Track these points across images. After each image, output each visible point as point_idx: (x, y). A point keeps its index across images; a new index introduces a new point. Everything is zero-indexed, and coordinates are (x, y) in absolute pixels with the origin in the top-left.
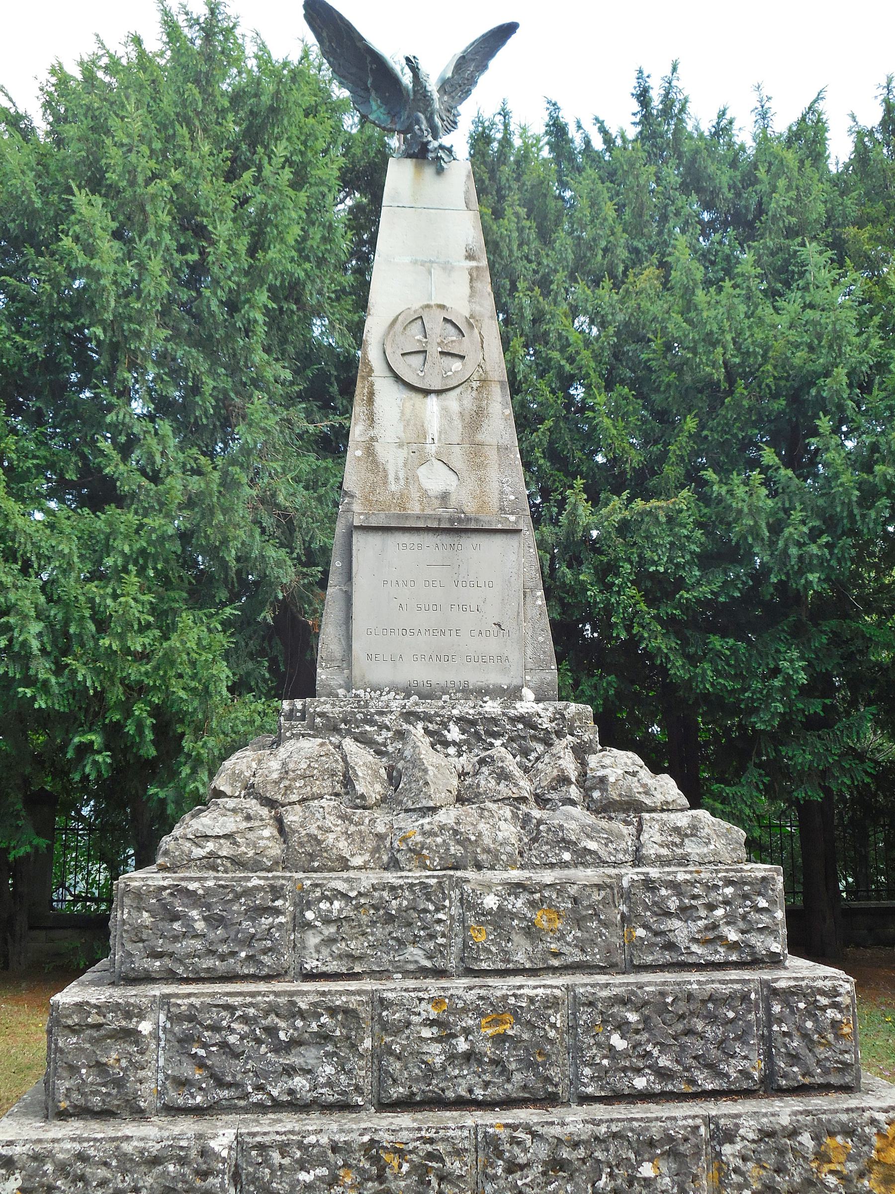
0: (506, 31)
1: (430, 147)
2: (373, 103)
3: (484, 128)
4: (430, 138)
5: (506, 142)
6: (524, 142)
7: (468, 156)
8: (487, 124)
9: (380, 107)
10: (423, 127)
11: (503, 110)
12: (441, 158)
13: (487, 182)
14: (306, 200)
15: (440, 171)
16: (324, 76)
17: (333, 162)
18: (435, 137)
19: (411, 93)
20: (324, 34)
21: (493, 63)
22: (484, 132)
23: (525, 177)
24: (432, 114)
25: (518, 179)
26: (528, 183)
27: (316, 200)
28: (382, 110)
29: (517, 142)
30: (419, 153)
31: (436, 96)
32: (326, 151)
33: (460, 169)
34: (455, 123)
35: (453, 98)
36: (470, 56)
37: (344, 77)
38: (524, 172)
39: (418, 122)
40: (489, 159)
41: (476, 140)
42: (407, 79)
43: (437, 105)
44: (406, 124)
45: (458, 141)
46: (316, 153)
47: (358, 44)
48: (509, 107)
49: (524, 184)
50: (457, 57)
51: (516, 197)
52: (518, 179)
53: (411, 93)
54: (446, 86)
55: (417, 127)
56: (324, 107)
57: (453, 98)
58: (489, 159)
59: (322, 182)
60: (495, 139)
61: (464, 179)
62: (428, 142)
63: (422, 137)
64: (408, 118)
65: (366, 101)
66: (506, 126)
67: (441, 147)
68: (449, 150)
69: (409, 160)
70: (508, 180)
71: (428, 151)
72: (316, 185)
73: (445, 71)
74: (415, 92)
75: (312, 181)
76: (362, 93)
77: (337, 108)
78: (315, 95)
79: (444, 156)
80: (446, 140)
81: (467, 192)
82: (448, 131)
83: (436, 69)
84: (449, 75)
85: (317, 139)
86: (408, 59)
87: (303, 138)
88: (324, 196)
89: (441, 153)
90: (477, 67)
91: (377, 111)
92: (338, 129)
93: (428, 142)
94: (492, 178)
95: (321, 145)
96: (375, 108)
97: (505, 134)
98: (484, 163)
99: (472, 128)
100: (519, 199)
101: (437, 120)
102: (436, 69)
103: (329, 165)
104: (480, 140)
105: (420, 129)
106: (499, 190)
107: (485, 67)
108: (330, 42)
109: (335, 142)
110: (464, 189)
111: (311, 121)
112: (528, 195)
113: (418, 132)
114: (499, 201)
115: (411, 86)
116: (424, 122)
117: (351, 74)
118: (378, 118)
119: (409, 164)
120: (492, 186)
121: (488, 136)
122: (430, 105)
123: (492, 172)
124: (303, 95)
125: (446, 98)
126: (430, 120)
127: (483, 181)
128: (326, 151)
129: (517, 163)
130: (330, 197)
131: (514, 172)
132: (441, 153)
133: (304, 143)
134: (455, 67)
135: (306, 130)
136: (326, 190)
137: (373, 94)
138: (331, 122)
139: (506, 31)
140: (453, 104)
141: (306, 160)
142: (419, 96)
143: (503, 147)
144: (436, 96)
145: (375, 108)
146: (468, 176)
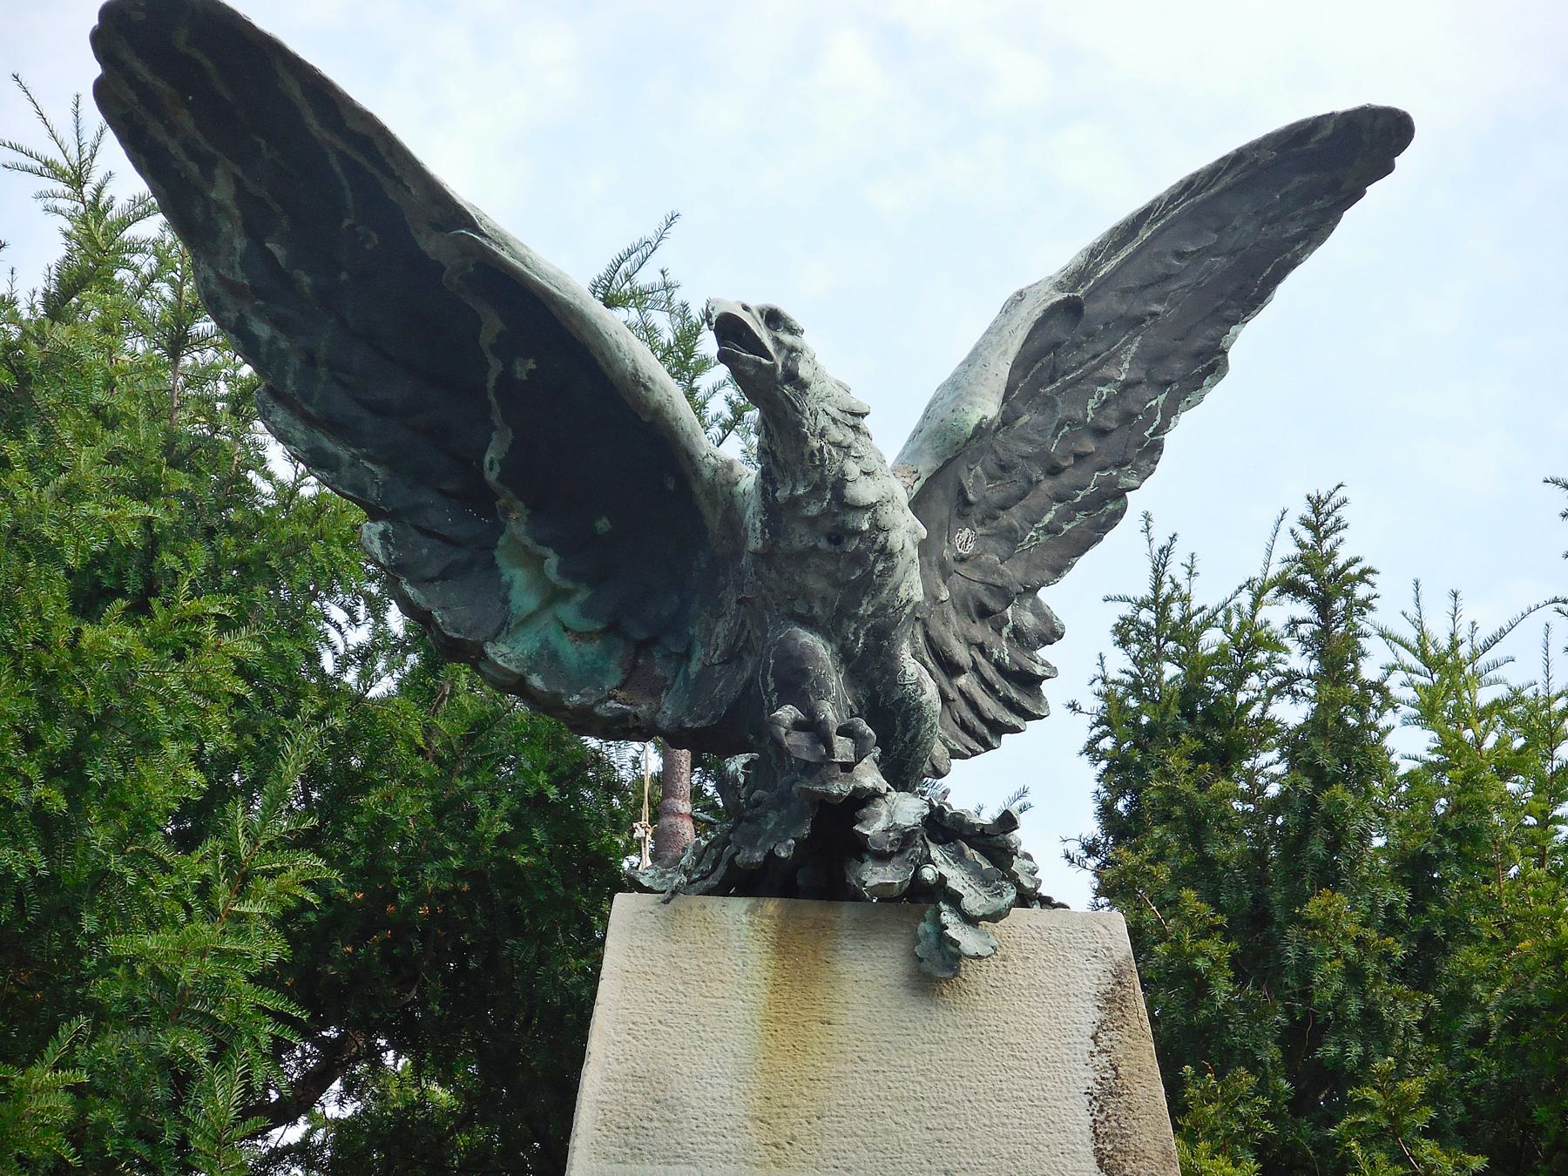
0: (1345, 154)
1: (874, 827)
2: (517, 577)
3: (1196, 667)
4: (869, 776)
5: (1338, 745)
6: (1450, 747)
7: (1092, 828)
8: (1212, 639)
9: (554, 596)
10: (830, 713)
11: (1312, 560)
12: (941, 892)
13: (1222, 989)
14: (63, 1105)
15: (936, 971)
16: (205, 374)
17: (242, 884)
18: (905, 769)
19: (752, 516)
20: (222, 192)
21: (1249, 344)
22: (1190, 692)
23: (1467, 957)
24: (882, 636)
25: (1419, 971)
26: (1492, 997)
27: (134, 1106)
28: (568, 612)
29: (1408, 744)
30: (806, 861)
31: (905, 530)
32: (197, 822)
33: (1062, 961)
34: (1030, 682)
35: (1011, 537)
36: (1110, 304)
37: (335, 427)
38: (1459, 930)
39: (795, 681)
40: (1227, 851)
41: (1147, 737)
42: (733, 452)
43: (912, 585)
44: (724, 690)
45: (1043, 783)
46: (141, 826)
47: (431, 245)
48: (1347, 549)
49: (1459, 1000)
50: (1031, 312)
51: (1413, 1086)
52: (1419, 971)
53: (752, 516)
54: (955, 469)
55: (787, 713)
56: (200, 555)
57: (1011, 537)
58: (1227, 851)
59: (173, 1002)
60: (1267, 727)
61: (1088, 1015)
62: (864, 799)
63: (822, 766)
64: (733, 657)
65: (472, 564)
66: (1335, 654)
67: (942, 827)
68: (993, 844)
69: (738, 907)
70: (1354, 974)
71: (860, 849)
72: (133, 1016)
73: (957, 388)
74: (776, 512)
75: (109, 991)
76: (441, 517)
77: (267, 567)
78: (145, 491)
79: (956, 879)
80: (972, 787)
81: (1107, 1095)
82: (984, 734)
83: (899, 364)
84: (987, 407)
85: (148, 744)
86: (730, 329)
87: (59, 738)
88: (181, 1078)
89: (941, 866)
90: (1153, 359)
91: (537, 624)
92: (282, 685)
93: (864, 799)
94: (1255, 963)
95: (172, 776)
96: (524, 599)
97: (1325, 706)
98: (1202, 873)
99: (1120, 663)
100: (1434, 1095)
101: (912, 666)
102: (899, 364)
103: (222, 892)
104: (1172, 735)
105: (812, 726)
106: (1302, 1035)
107: (1212, 364)
108: (255, 230)
109: (265, 757)
110: (1087, 1077)
111: (112, 635)
112: (1490, 1068)
113: (796, 742)
114: (1300, 1104)
115: (748, 476)
116: (835, 680)
117: (380, 410)
118: (547, 659)
119: (739, 922)
120: (1255, 1013)
121: (1223, 716)
122: (869, 585)
123: (1257, 935)
124: (72, 494)
125: (965, 540)
126: (871, 672)
127: (1199, 986)
128: (197, 822)
129: (1414, 869)
130: (222, 1095)
131: (1393, 925)
132: (941, 866)
133: (67, 770)
134: (1023, 364)
135: (83, 696)
136: (200, 1051)
137: (517, 525)
138: (243, 645)
139: (1345, 154)
140: (1013, 573)
141: (76, 870)
142: (801, 538)
143: (1322, 780)
144: (905, 530)
145: (524, 599)
146: (1112, 1001)
